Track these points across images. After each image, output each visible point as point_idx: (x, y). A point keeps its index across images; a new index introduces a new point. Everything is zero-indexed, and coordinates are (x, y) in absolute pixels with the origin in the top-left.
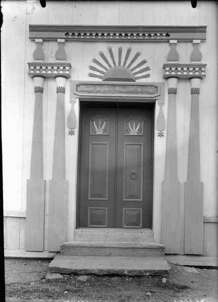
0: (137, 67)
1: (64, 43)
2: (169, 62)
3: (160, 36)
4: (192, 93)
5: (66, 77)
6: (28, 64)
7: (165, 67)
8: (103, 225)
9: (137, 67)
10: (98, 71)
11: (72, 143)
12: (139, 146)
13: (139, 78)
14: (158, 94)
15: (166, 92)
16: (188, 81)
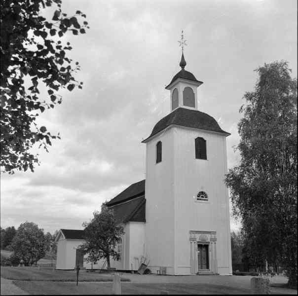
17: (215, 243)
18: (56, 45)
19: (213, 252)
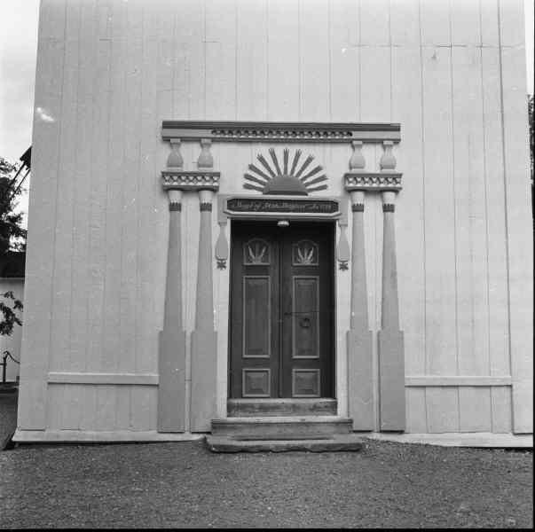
0: (310, 175)
1: (391, 146)
2: (201, 169)
3: (299, 135)
4: (384, 211)
5: (214, 190)
6: (163, 173)
7: (164, 174)
8: (263, 393)
9: (310, 175)
10: (256, 180)
11: (222, 280)
12: (313, 281)
13: (311, 190)
14: (339, 212)
15: (350, 208)
16: (195, 194)
17: (388, 208)
18: (245, 172)
19: (374, 290)
